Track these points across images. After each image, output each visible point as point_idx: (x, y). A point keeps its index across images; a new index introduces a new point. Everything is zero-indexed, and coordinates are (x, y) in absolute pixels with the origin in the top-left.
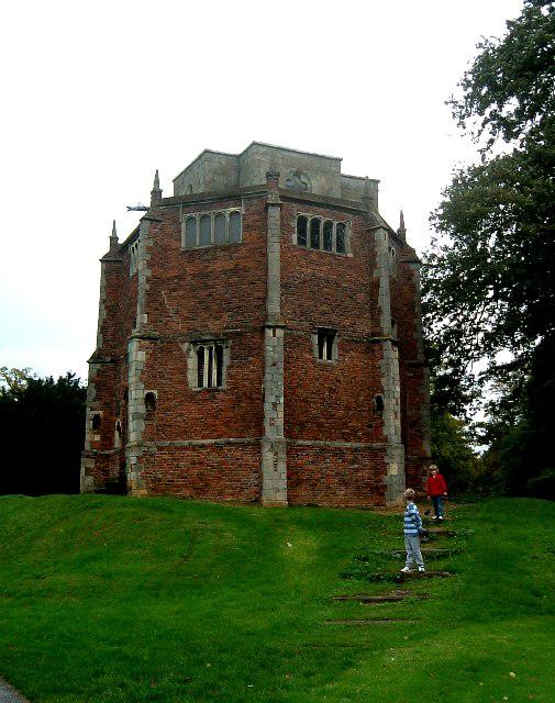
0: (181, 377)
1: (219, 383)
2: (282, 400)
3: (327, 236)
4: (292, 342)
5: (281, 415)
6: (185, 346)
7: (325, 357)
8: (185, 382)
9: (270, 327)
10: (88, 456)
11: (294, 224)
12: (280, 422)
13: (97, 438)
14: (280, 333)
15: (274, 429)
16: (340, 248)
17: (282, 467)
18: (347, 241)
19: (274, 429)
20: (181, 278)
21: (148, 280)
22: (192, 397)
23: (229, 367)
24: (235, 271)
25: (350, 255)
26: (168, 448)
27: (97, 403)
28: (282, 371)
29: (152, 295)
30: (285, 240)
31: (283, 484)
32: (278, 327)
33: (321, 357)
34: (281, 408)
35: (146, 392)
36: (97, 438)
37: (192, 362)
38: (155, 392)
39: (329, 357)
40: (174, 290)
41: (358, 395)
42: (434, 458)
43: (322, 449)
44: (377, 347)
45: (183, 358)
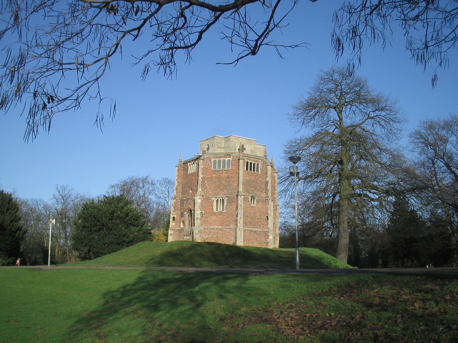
0: (211, 207)
1: (223, 210)
2: (242, 216)
3: (254, 167)
4: (245, 199)
5: (242, 220)
6: (213, 199)
7: (256, 171)
8: (212, 209)
9: (239, 195)
10: (171, 230)
11: (245, 164)
12: (242, 222)
13: (174, 224)
14: (242, 197)
15: (241, 221)
16: (257, 171)
17: (242, 235)
18: (259, 168)
19: (241, 221)
20: (211, 178)
21: (202, 178)
22: (215, 214)
23: (226, 206)
24: (228, 177)
25: (260, 173)
26: (207, 229)
27: (174, 213)
28: (243, 208)
29: (203, 182)
30: (243, 168)
31: (242, 240)
32: (242, 195)
33: (251, 204)
34: (242, 218)
35: (201, 211)
36: (174, 224)
37: (215, 203)
38: (203, 212)
39: (253, 204)
40: (209, 181)
41: (261, 215)
42: (349, 147)
43: (251, 231)
44: (267, 201)
45: (212, 202)
